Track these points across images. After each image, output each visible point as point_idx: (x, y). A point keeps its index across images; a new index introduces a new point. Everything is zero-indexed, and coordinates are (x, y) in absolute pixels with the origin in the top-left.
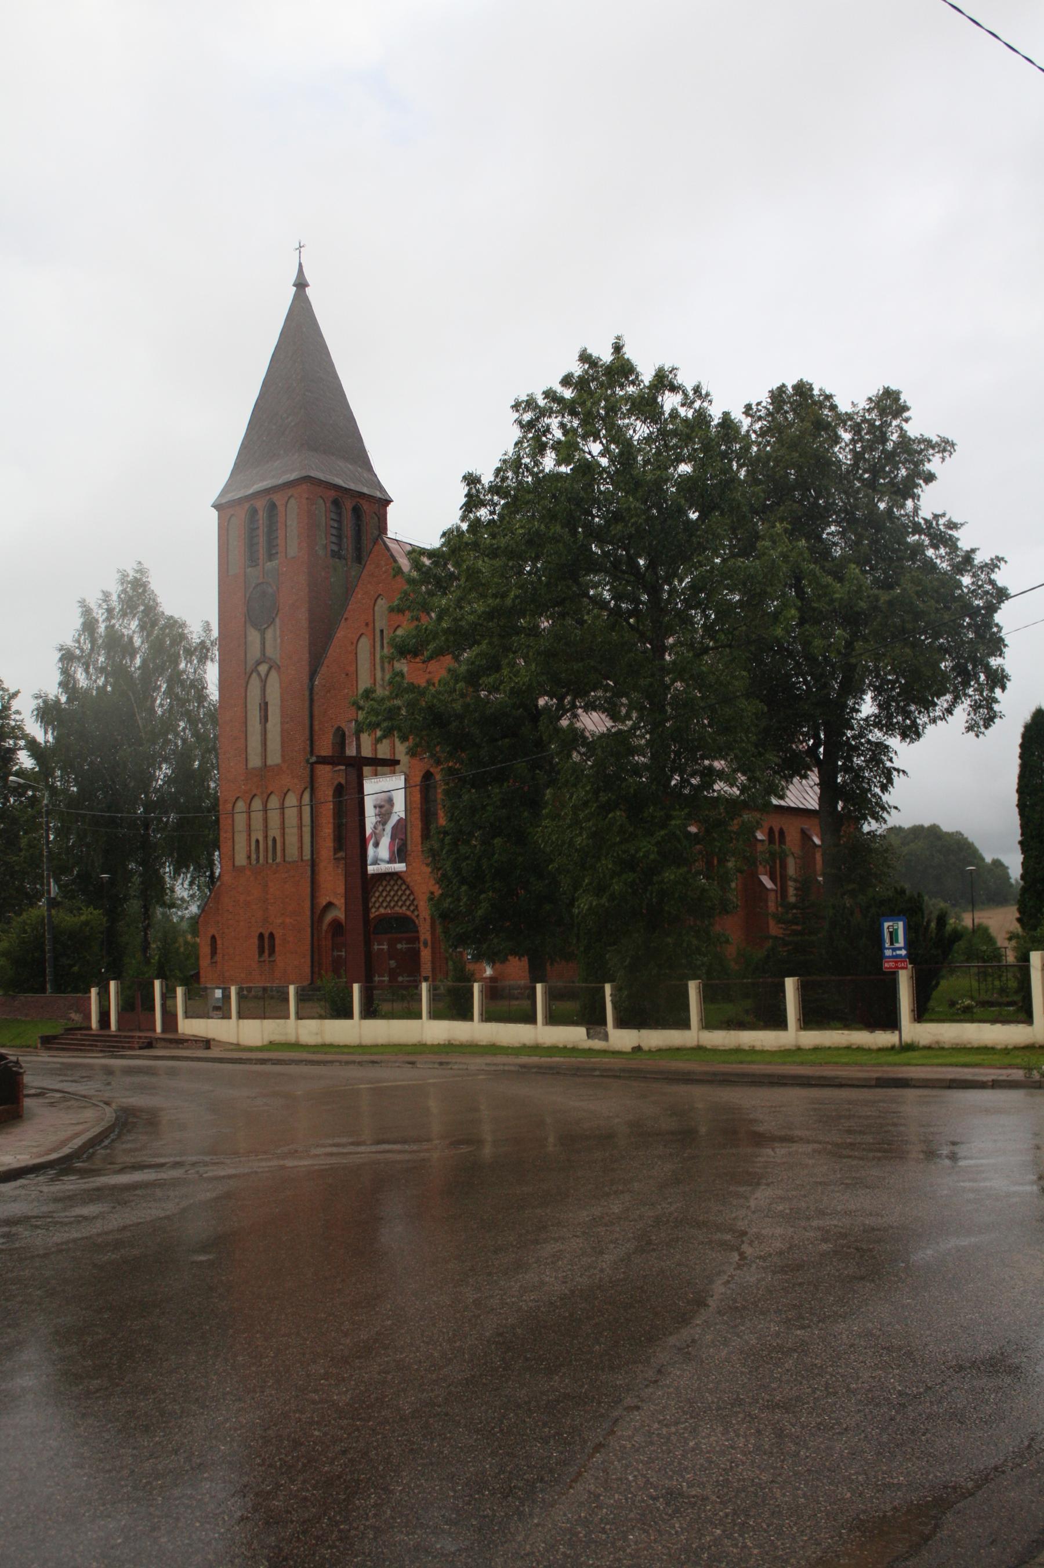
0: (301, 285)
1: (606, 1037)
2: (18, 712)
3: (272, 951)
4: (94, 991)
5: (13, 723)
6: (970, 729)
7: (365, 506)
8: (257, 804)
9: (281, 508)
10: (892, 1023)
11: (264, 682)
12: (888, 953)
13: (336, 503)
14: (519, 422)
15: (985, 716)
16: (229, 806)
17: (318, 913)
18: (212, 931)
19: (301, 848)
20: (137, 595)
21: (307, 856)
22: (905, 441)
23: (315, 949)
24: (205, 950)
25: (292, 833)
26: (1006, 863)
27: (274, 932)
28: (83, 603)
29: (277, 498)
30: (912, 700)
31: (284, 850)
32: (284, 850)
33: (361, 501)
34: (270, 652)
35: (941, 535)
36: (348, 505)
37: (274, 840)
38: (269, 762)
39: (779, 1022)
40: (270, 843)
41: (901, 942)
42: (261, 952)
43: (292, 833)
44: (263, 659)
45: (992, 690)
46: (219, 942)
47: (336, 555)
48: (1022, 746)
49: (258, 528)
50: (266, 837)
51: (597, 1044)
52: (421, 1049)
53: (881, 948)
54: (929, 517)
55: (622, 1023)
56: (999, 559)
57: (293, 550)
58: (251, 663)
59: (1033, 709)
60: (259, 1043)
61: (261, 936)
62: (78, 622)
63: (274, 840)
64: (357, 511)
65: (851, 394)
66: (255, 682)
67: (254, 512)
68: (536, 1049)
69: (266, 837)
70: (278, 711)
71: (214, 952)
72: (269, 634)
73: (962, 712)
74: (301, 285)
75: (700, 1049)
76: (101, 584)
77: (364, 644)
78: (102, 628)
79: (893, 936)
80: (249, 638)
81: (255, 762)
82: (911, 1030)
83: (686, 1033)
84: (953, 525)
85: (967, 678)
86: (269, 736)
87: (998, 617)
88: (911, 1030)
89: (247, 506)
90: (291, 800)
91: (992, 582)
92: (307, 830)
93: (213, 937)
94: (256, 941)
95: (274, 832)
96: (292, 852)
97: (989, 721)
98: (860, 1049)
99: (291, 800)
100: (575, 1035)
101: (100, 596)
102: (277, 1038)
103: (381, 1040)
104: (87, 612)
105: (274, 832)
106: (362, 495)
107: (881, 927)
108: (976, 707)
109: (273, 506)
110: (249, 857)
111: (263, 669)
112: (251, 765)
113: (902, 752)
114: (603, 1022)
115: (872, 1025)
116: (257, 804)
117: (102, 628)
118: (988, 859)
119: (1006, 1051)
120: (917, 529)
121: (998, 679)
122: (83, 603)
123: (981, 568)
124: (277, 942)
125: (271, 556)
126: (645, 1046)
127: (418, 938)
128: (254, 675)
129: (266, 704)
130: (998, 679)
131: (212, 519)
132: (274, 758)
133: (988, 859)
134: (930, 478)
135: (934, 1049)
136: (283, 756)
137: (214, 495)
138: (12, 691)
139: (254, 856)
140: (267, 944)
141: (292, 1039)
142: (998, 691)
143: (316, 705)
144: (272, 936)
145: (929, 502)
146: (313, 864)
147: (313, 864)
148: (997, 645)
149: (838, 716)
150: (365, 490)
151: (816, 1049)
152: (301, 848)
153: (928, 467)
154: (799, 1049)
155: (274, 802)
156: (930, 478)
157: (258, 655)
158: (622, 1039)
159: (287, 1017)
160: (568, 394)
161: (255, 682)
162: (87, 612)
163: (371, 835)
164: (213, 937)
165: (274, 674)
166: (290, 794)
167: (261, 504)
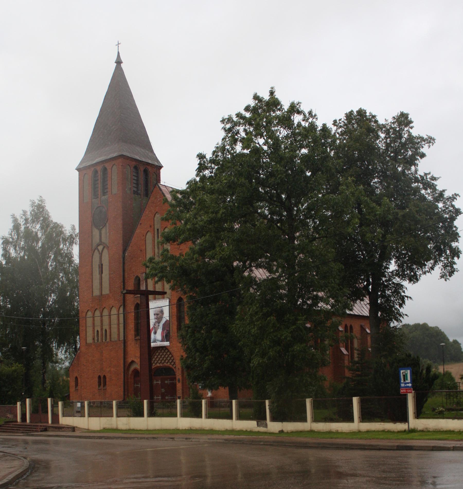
0: (119, 62)
1: (266, 426)
3: (105, 384)
4: (19, 404)
7: (150, 169)
8: (98, 313)
9: (109, 170)
11: (101, 254)
12: (403, 385)
13: (136, 168)
21: (122, 338)
23: (126, 383)
24: (72, 384)
26: (460, 342)
27: (106, 375)
31: (110, 335)
32: (110, 335)
33: (148, 167)
34: (103, 240)
35: (428, 183)
36: (142, 168)
37: (106, 330)
38: (103, 293)
39: (350, 419)
40: (104, 332)
41: (409, 380)
42: (100, 384)
44: (101, 243)
45: (453, 258)
46: (79, 380)
47: (136, 193)
49: (98, 180)
50: (102, 329)
51: (262, 429)
53: (399, 383)
55: (274, 419)
56: (456, 195)
57: (115, 191)
58: (94, 245)
60: (99, 429)
61: (99, 377)
64: (146, 171)
65: (384, 115)
66: (96, 255)
67: (96, 172)
68: (232, 432)
69: (102, 329)
70: (108, 268)
71: (77, 385)
72: (103, 231)
73: (438, 269)
74: (119, 62)
75: (311, 431)
76: (22, 207)
78: (22, 228)
79: (405, 377)
80: (94, 233)
81: (96, 293)
82: (414, 423)
83: (305, 424)
84: (434, 179)
87: (456, 223)
88: (414, 423)
89: (93, 169)
90: (114, 311)
92: (122, 326)
94: (97, 379)
95: (106, 327)
96: (115, 336)
97: (451, 273)
99: (114, 311)
100: (251, 425)
101: (22, 212)
105: (106, 327)
106: (148, 164)
108: (445, 266)
109: (105, 169)
110: (94, 339)
111: (100, 248)
112: (94, 294)
113: (409, 288)
114: (265, 419)
115: (395, 420)
116: (98, 313)
117: (22, 228)
120: (417, 180)
121: (456, 253)
123: (448, 199)
124: (107, 380)
125: (104, 193)
126: (285, 430)
127: (175, 378)
129: (102, 265)
130: (456, 253)
132: (106, 291)
136: (110, 290)
139: (96, 338)
140: (102, 381)
141: (114, 426)
142: (456, 258)
144: (105, 377)
145: (423, 167)
146: (125, 342)
147: (125, 342)
148: (455, 236)
149: (378, 271)
150: (150, 162)
153: (422, 150)
154: (360, 432)
155: (106, 312)
157: (98, 241)
158: (274, 427)
161: (96, 255)
163: (153, 328)
166: (113, 308)
167: (99, 168)
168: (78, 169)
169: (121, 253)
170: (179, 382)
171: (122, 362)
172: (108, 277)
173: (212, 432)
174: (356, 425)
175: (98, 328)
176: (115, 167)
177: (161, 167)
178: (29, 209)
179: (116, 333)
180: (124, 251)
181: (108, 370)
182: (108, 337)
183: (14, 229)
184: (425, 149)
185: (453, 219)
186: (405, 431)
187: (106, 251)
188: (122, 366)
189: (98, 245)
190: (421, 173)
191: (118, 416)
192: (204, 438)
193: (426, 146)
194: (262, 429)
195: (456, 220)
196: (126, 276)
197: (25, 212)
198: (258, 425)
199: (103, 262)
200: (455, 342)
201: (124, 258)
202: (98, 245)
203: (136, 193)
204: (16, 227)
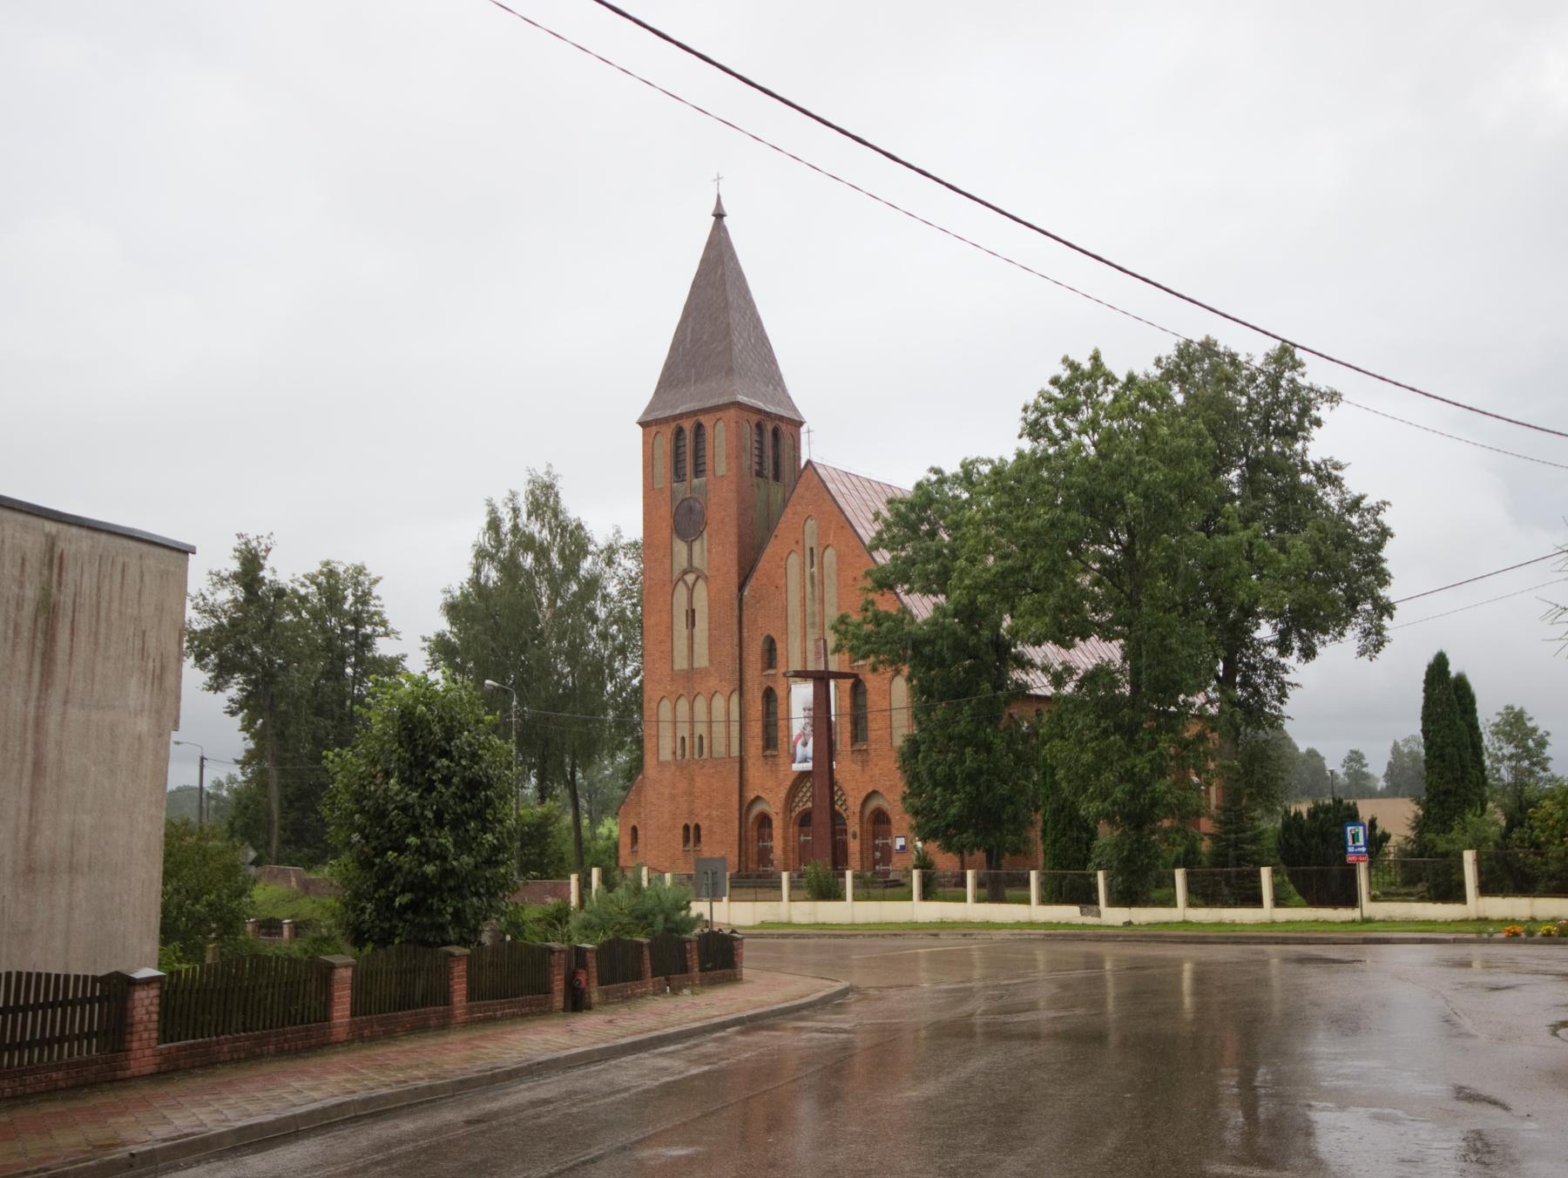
0: (719, 216)
1: (1098, 914)
2: (378, 598)
4: (574, 878)
5: (372, 609)
6: (1361, 654)
7: (783, 427)
8: (683, 705)
9: (708, 430)
10: (1351, 901)
11: (691, 591)
12: (1350, 849)
13: (759, 426)
14: (1025, 419)
15: (1375, 641)
16: (654, 705)
17: (745, 806)
18: (633, 822)
19: (729, 746)
20: (544, 500)
21: (735, 752)
22: (1295, 390)
23: (742, 839)
24: (626, 840)
25: (719, 729)
26: (1322, 754)
28: (490, 503)
29: (703, 419)
30: (1308, 623)
31: (711, 747)
32: (711, 747)
34: (697, 562)
35: (1328, 476)
36: (769, 427)
37: (701, 738)
38: (696, 665)
39: (1256, 901)
40: (696, 740)
41: (1361, 842)
42: (686, 840)
43: (719, 729)
44: (690, 569)
45: (1380, 618)
46: (640, 832)
47: (759, 474)
48: (1426, 682)
50: (692, 735)
51: (1090, 920)
52: (915, 928)
53: (1345, 847)
54: (1318, 460)
55: (1112, 903)
56: (1384, 503)
57: (721, 469)
58: (676, 574)
59: (1435, 652)
60: (751, 923)
61: (686, 828)
62: (483, 521)
63: (701, 738)
64: (776, 433)
65: (1254, 351)
66: (681, 592)
67: (680, 431)
68: (1032, 924)
69: (692, 735)
72: (697, 546)
73: (1352, 636)
74: (719, 216)
75: (1185, 922)
76: (508, 484)
77: (794, 561)
78: (506, 526)
79: (1355, 838)
80: (676, 549)
81: (681, 663)
82: (1369, 908)
83: (1173, 910)
84: (1338, 467)
85: (1353, 603)
86: (696, 640)
87: (1383, 554)
88: (1369, 908)
89: (673, 425)
90: (719, 703)
91: (1376, 522)
92: (735, 728)
93: (634, 829)
94: (681, 831)
96: (720, 749)
97: (1378, 646)
98: (1326, 922)
99: (719, 703)
100: (1069, 913)
101: (507, 494)
102: (770, 918)
103: (872, 919)
104: (493, 511)
106: (781, 418)
107: (1345, 833)
108: (1366, 633)
109: (699, 428)
111: (690, 578)
112: (677, 667)
113: (1295, 668)
114: (1096, 903)
115: (1335, 903)
116: (683, 705)
117: (506, 526)
118: (1302, 749)
119: (1447, 923)
120: (1306, 469)
121: (1386, 609)
122: (490, 503)
123: (1368, 510)
124: (703, 833)
125: (698, 472)
126: (1135, 921)
127: (845, 831)
128: (681, 584)
129: (693, 611)
130: (1386, 609)
131: (635, 436)
132: (702, 661)
133: (1302, 749)
134: (1318, 422)
135: (1387, 922)
136: (711, 661)
137: (638, 410)
138: (373, 576)
139: (679, 752)
140: (692, 834)
141: (785, 919)
142: (1386, 618)
143: (745, 613)
144: (697, 827)
145: (1317, 447)
146: (742, 761)
147: (742, 761)
148: (1383, 579)
149: (1236, 638)
151: (1288, 922)
152: (729, 746)
153: (1314, 413)
154: (1273, 922)
155: (700, 704)
156: (1318, 422)
157: (685, 565)
158: (1114, 916)
159: (780, 899)
160: (1056, 393)
161: (681, 592)
162: (493, 511)
163: (799, 736)
164: (634, 829)
165: (701, 583)
166: (718, 696)
167: (688, 425)
168: (644, 424)
169: (735, 590)
170: (855, 836)
171: (735, 797)
172: (706, 633)
173: (989, 925)
174: (1268, 912)
175: (684, 731)
176: (720, 425)
177: (801, 424)
178: (522, 490)
179: (723, 741)
180: (741, 587)
181: (705, 813)
182: (706, 750)
183: (489, 528)
184: (1322, 411)
185: (1378, 546)
186: (1353, 921)
187: (701, 584)
188: (737, 807)
189: (685, 572)
190: (1313, 457)
191: (791, 900)
192: (1005, 933)
193: (1325, 407)
194: (1090, 920)
195: (1391, 553)
196: (745, 635)
197: (513, 496)
198: (1082, 913)
199: (696, 606)
200: (1312, 754)
201: (741, 601)
202: (685, 572)
203: (759, 474)
204: (494, 525)
